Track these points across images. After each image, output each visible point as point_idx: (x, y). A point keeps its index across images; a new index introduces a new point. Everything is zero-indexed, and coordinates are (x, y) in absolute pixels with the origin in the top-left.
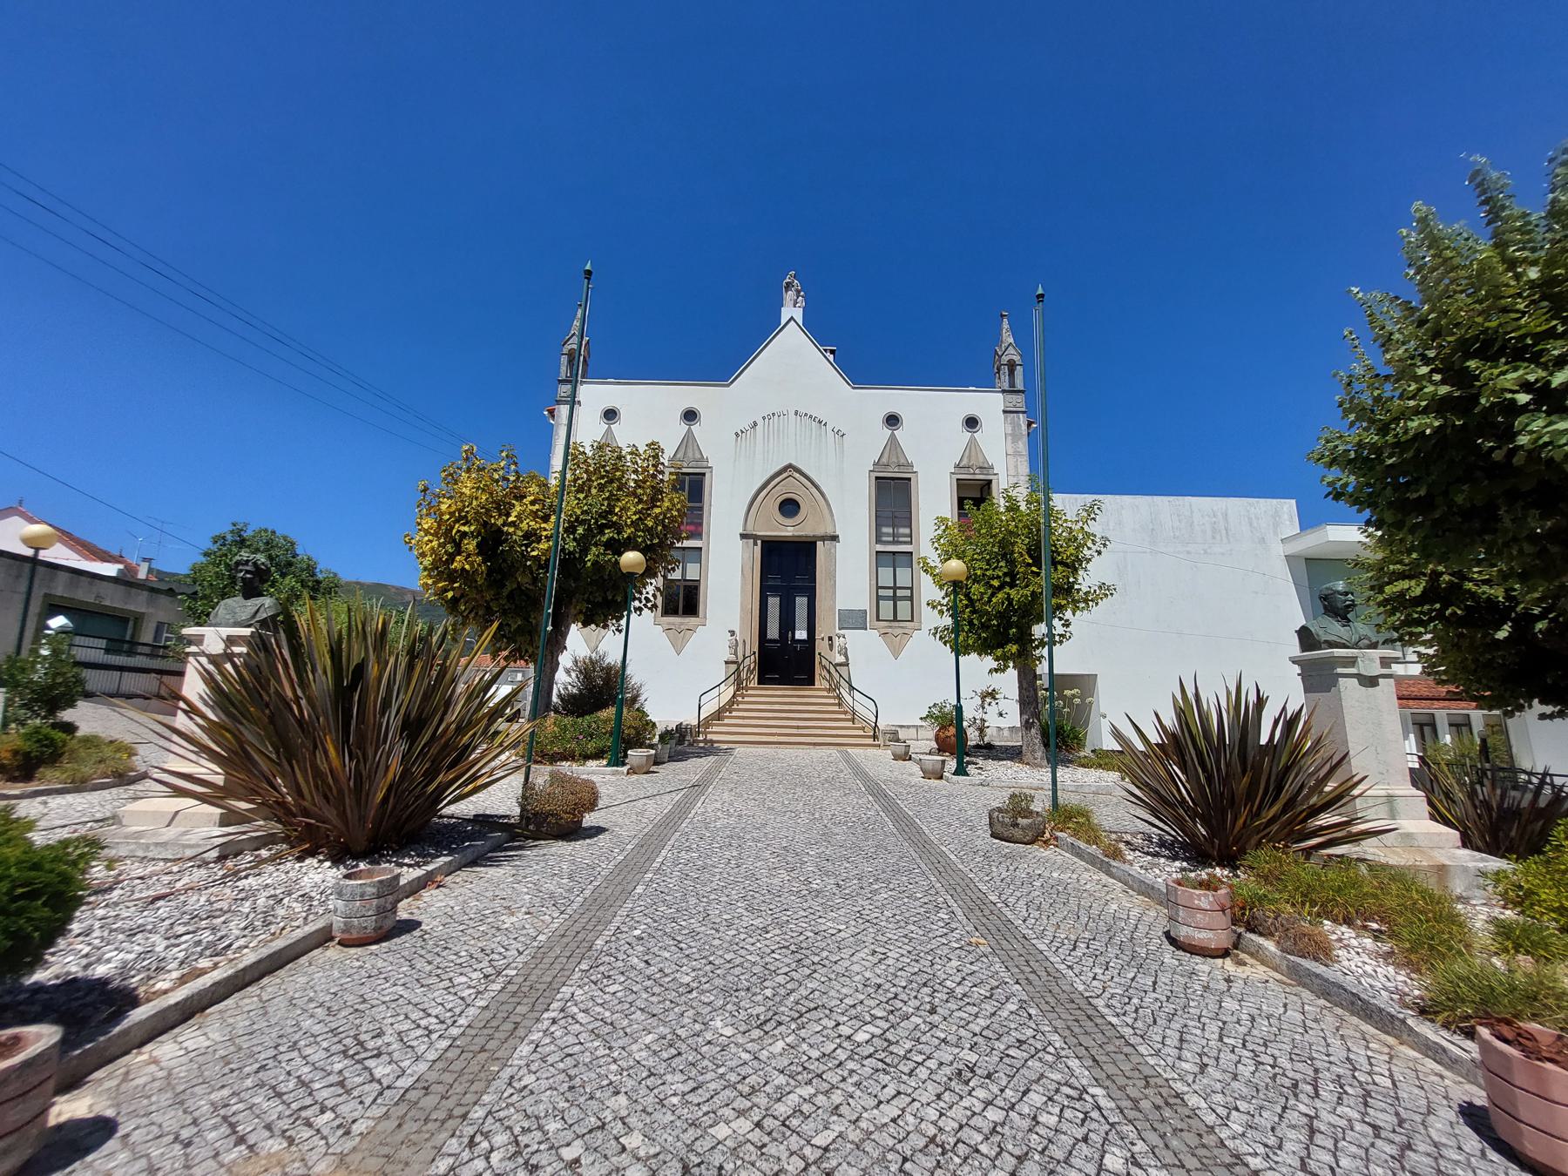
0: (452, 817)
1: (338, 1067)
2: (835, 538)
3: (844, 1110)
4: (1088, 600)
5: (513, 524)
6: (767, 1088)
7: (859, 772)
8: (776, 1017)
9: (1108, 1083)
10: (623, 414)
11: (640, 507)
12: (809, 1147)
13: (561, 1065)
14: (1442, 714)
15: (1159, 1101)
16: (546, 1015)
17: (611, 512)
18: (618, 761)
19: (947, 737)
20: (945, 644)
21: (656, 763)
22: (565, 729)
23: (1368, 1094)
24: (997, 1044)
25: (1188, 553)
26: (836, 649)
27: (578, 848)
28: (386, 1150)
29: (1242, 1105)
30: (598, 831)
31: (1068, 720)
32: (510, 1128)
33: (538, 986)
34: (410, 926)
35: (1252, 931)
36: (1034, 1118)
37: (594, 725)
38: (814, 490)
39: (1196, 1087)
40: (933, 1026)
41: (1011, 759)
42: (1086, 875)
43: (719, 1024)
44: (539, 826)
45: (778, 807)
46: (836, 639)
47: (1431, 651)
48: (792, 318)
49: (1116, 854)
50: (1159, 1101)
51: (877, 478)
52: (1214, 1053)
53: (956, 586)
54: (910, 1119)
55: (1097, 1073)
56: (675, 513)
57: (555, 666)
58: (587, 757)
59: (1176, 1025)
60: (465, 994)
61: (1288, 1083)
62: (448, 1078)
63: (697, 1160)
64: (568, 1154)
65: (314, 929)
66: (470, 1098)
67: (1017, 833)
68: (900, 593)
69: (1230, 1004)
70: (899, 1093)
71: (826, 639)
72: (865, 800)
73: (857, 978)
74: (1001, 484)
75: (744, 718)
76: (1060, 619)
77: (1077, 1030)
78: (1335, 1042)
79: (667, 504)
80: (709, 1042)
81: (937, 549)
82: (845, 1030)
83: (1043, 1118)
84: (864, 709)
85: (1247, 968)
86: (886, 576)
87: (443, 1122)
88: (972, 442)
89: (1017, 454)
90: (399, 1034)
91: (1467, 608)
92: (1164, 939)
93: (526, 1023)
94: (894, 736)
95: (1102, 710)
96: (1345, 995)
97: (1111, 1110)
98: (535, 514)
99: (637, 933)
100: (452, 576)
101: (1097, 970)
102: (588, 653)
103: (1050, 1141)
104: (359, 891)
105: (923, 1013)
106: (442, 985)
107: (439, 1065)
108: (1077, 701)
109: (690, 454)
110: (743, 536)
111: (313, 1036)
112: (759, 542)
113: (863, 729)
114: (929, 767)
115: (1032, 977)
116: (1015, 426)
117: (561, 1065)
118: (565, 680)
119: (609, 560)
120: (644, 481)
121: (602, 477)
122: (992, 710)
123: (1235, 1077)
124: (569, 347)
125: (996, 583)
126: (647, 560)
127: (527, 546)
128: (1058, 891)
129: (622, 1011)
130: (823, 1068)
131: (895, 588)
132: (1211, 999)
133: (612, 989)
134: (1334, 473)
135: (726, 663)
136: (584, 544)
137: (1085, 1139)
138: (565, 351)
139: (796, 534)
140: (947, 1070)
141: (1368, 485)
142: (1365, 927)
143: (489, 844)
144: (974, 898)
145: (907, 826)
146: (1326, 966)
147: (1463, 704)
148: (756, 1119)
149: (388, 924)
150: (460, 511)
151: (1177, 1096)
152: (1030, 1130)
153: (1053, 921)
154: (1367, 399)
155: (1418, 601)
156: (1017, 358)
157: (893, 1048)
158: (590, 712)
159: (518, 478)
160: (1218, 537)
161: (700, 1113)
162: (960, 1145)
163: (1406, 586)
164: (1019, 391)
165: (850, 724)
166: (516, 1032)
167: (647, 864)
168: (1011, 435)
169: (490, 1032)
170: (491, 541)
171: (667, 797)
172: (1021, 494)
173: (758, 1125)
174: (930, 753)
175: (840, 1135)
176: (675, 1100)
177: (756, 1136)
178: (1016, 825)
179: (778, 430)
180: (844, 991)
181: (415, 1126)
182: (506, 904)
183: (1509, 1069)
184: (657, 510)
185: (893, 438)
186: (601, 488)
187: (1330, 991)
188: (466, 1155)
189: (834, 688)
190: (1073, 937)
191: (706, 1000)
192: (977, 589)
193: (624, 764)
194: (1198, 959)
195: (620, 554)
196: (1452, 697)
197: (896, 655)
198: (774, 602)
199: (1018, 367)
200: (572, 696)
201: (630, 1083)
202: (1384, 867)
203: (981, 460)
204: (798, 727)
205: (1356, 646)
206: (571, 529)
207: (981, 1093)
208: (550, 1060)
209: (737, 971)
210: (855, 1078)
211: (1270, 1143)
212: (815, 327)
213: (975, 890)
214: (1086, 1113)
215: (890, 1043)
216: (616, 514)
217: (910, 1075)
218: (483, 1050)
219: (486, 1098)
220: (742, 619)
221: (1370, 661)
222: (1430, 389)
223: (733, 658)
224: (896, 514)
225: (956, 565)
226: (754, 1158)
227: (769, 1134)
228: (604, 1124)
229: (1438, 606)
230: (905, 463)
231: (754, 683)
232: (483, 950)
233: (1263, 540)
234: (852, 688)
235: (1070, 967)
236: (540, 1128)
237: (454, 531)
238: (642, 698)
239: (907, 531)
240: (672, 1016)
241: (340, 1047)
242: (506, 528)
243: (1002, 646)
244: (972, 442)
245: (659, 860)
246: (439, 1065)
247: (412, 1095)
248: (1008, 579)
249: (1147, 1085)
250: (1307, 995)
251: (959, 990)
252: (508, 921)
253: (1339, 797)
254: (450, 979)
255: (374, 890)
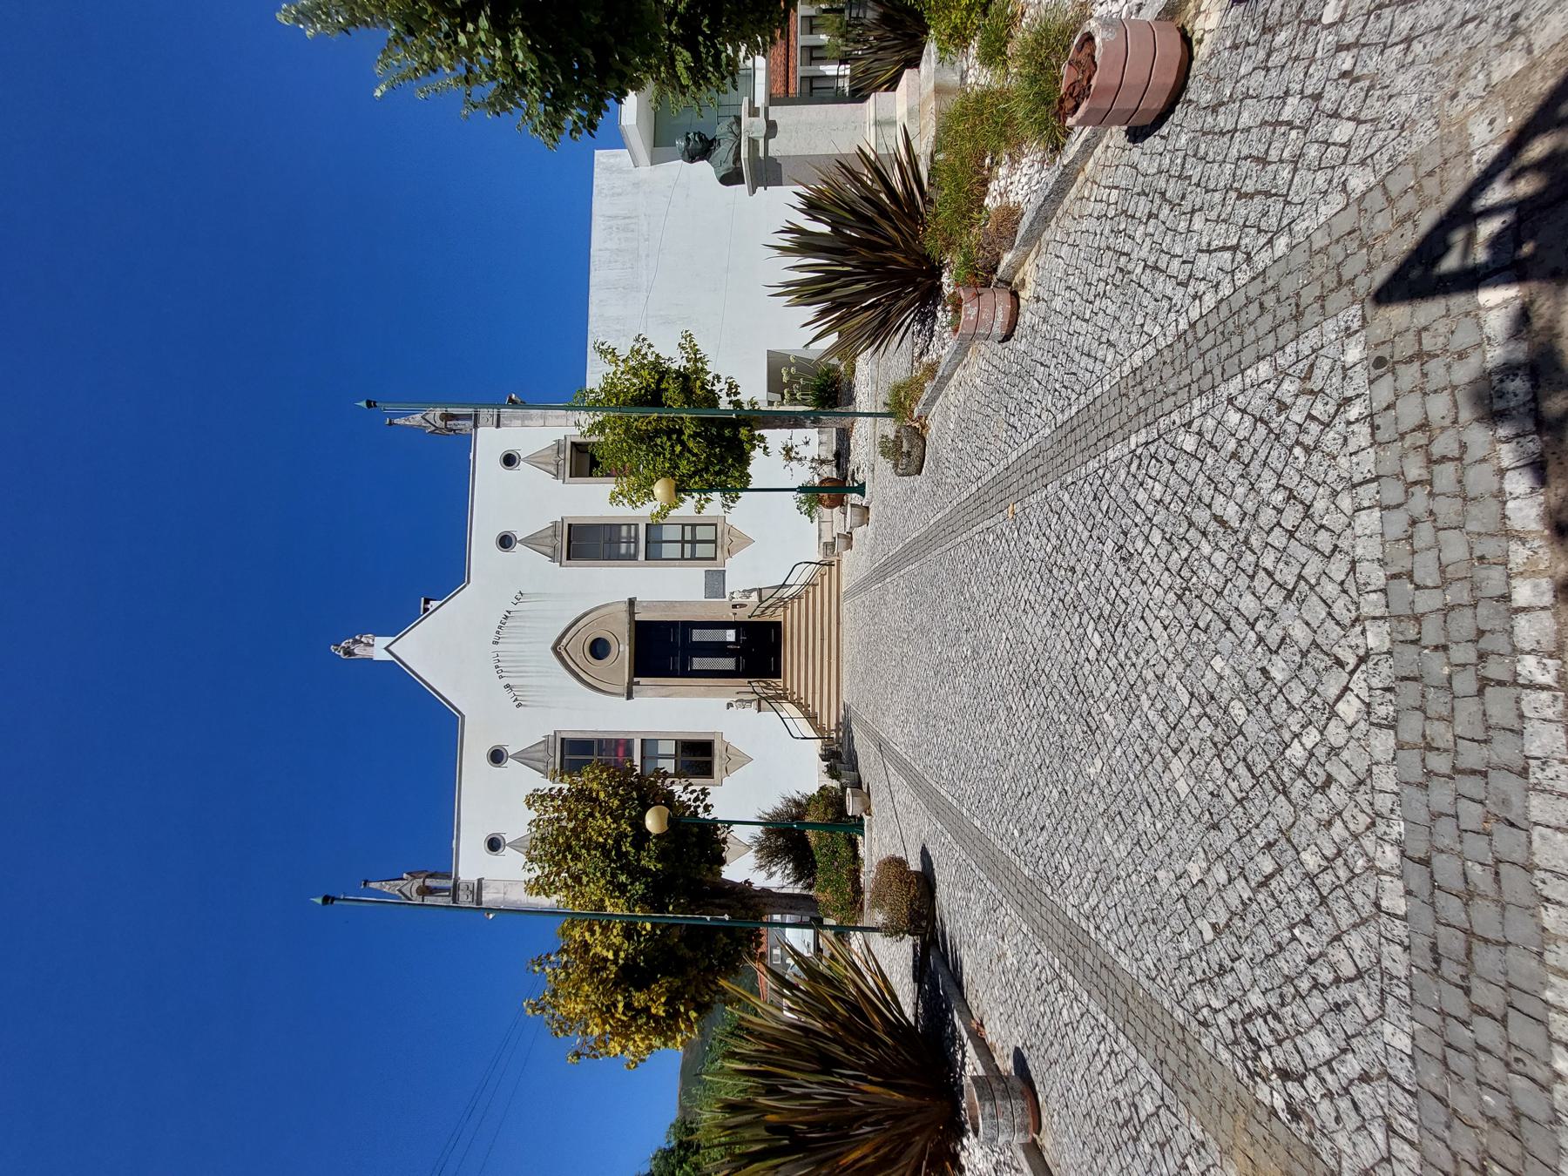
0: (916, 1004)
1: (1147, 1148)
2: (632, 602)
3: (1159, 670)
4: (696, 357)
5: (616, 954)
6: (1145, 737)
7: (862, 586)
8: (1084, 715)
9: (1126, 429)
10: (491, 830)
11: (597, 815)
12: (1192, 710)
13: (1135, 928)
14: (802, 39)
15: (1139, 389)
16: (1093, 936)
17: (603, 846)
18: (859, 824)
20: (738, 498)
21: (860, 787)
22: (829, 881)
23: (1124, 212)
24: (1097, 519)
25: (648, 256)
26: (744, 600)
27: (942, 877)
28: (1215, 1108)
29: (1139, 320)
30: (925, 854)
31: (810, 380)
32: (1190, 985)
33: (1068, 939)
34: (1019, 1059)
35: (995, 270)
36: (1158, 502)
37: (824, 851)
38: (581, 624)
39: (1126, 355)
40: (1085, 572)
41: (849, 439)
42: (952, 398)
43: (1092, 770)
44: (922, 917)
45: (899, 671)
46: (735, 601)
47: (743, 48)
48: (387, 649)
49: (932, 369)
50: (1139, 389)
51: (568, 558)
52: (1099, 331)
53: (681, 489)
54: (1163, 613)
55: (1119, 435)
56: (605, 775)
57: (766, 892)
58: (856, 857)
59: (1077, 357)
60: (1078, 1013)
61: (1119, 276)
62: (1151, 1039)
63: (1207, 815)
64: (1209, 935)
65: (1026, 1163)
66: (1167, 1021)
67: (916, 452)
68: (688, 537)
69: (1057, 304)
70: (1142, 618)
71: (735, 610)
72: (890, 586)
73: (1048, 633)
74: (575, 434)
75: (814, 693)
76: (713, 385)
77: (1084, 444)
78: (1085, 225)
79: (595, 786)
80: (1109, 783)
82: (1092, 655)
83: (1157, 495)
84: (802, 576)
85: (1028, 279)
86: (671, 550)
87: (1189, 1049)
88: (530, 460)
89: (544, 418)
90: (1116, 1083)
91: (703, 14)
92: (1005, 344)
93: (1100, 955)
94: (829, 546)
95: (800, 347)
96: (1047, 206)
97: (1147, 433)
98: (606, 929)
99: (1016, 834)
100: (673, 1015)
101: (1033, 412)
102: (751, 853)
103: (1175, 493)
104: (988, 1121)
105: (1075, 580)
106: (1071, 1034)
107: (1141, 1045)
108: (793, 370)
109: (540, 755)
110: (630, 696)
111: (1121, 1171)
112: (636, 680)
113: (822, 576)
114: (857, 519)
115: (1040, 471)
117: (1135, 928)
118: (778, 880)
119: (655, 844)
120: (570, 811)
121: (565, 857)
122: (803, 451)
123: (1116, 319)
126: (656, 804)
127: (639, 935)
128: (966, 427)
129: (1086, 861)
130: (1124, 682)
131: (683, 542)
132: (1053, 319)
133: (1067, 867)
134: (569, 120)
136: (637, 872)
137: (1173, 463)
140: (1122, 570)
141: (579, 98)
142: (990, 169)
143: (941, 969)
144: (973, 506)
145: (914, 551)
146: (1023, 214)
147: (792, 19)
148: (1171, 754)
149: (1018, 1084)
150: (602, 1013)
151: (1134, 372)
152: (1167, 508)
153: (992, 440)
154: (491, 88)
155: (696, 56)
156: (439, 411)
157: (1106, 613)
158: (812, 855)
159: (566, 951)
160: (632, 226)
161: (1169, 804)
162: (1182, 573)
163: (682, 64)
165: (818, 588)
166: (1110, 968)
167: (954, 811)
169: (1110, 993)
170: (633, 976)
171: (892, 779)
172: (586, 419)
173: (1175, 752)
174: (845, 514)
175: (1180, 679)
176: (1159, 826)
177: (1185, 755)
178: (909, 454)
180: (1059, 647)
181: (1194, 1077)
182: (995, 960)
183: (1098, 111)
184: (602, 795)
186: (577, 857)
187: (1044, 217)
188: (1215, 1032)
190: (1005, 426)
191: (1073, 778)
192: (684, 467)
193: (861, 819)
194: (1021, 320)
195: (650, 833)
196: (786, 35)
197: (749, 541)
198: (698, 663)
200: (795, 869)
201: (1147, 865)
202: (937, 139)
203: (550, 452)
204: (822, 639)
205: (738, 137)
206: (622, 888)
207: (1140, 544)
208: (1131, 938)
209: (1047, 745)
210: (1132, 654)
211: (1167, 306)
212: (398, 621)
213: (967, 503)
214: (1152, 457)
215: (1101, 615)
216: (606, 840)
217: (1127, 604)
218: (1125, 1002)
219: (1167, 1005)
221: (753, 127)
222: (482, 36)
223: (754, 704)
224: (607, 539)
225: (660, 489)
226: (1203, 763)
227: (1182, 744)
228: (1182, 896)
229: (701, 39)
231: (780, 682)
232: (1038, 989)
233: (636, 185)
235: (1031, 435)
236: (1189, 957)
237: (624, 1018)
238: (797, 797)
239: (624, 529)
240: (1088, 813)
241: (1130, 1143)
242: (621, 962)
244: (530, 460)
245: (950, 799)
246: (1141, 1045)
247: (1168, 1076)
248: (674, 437)
249: (1126, 395)
250: (1047, 235)
251: (1054, 541)
252: (1011, 960)
253: (877, 170)
254: (1066, 1025)
255: (987, 1104)
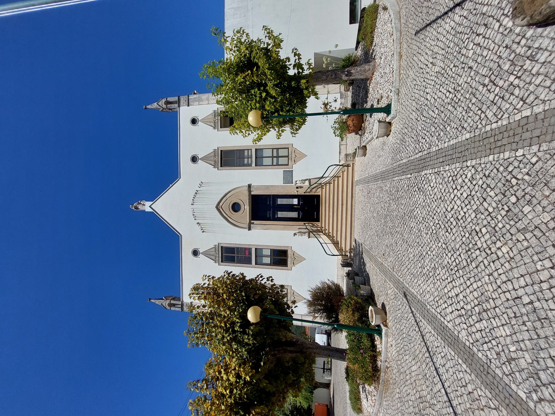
19: (353, 125)
26: (302, 185)
38: (228, 196)
48: (150, 207)
71: (297, 190)
81: (249, 134)
84: (332, 172)
86: (267, 161)
109: (213, 253)
110: (250, 229)
112: (252, 221)
114: (383, 131)
116: (195, 100)
124: (167, 306)
125: (264, 95)
131: (273, 157)
135: (309, 237)
138: (169, 308)
139: (248, 204)
156: (164, 100)
164: (179, 99)
165: (340, 179)
168: (199, 102)
179: (201, 213)
185: (202, 159)
189: (321, 186)
198: (280, 214)
199: (168, 100)
203: (211, 116)
204: (342, 205)
212: (153, 196)
220: (288, 230)
223: (307, 234)
230: (214, 153)
231: (319, 224)
234: (322, 177)
239: (246, 152)
243: (302, 90)
248: (262, 88)
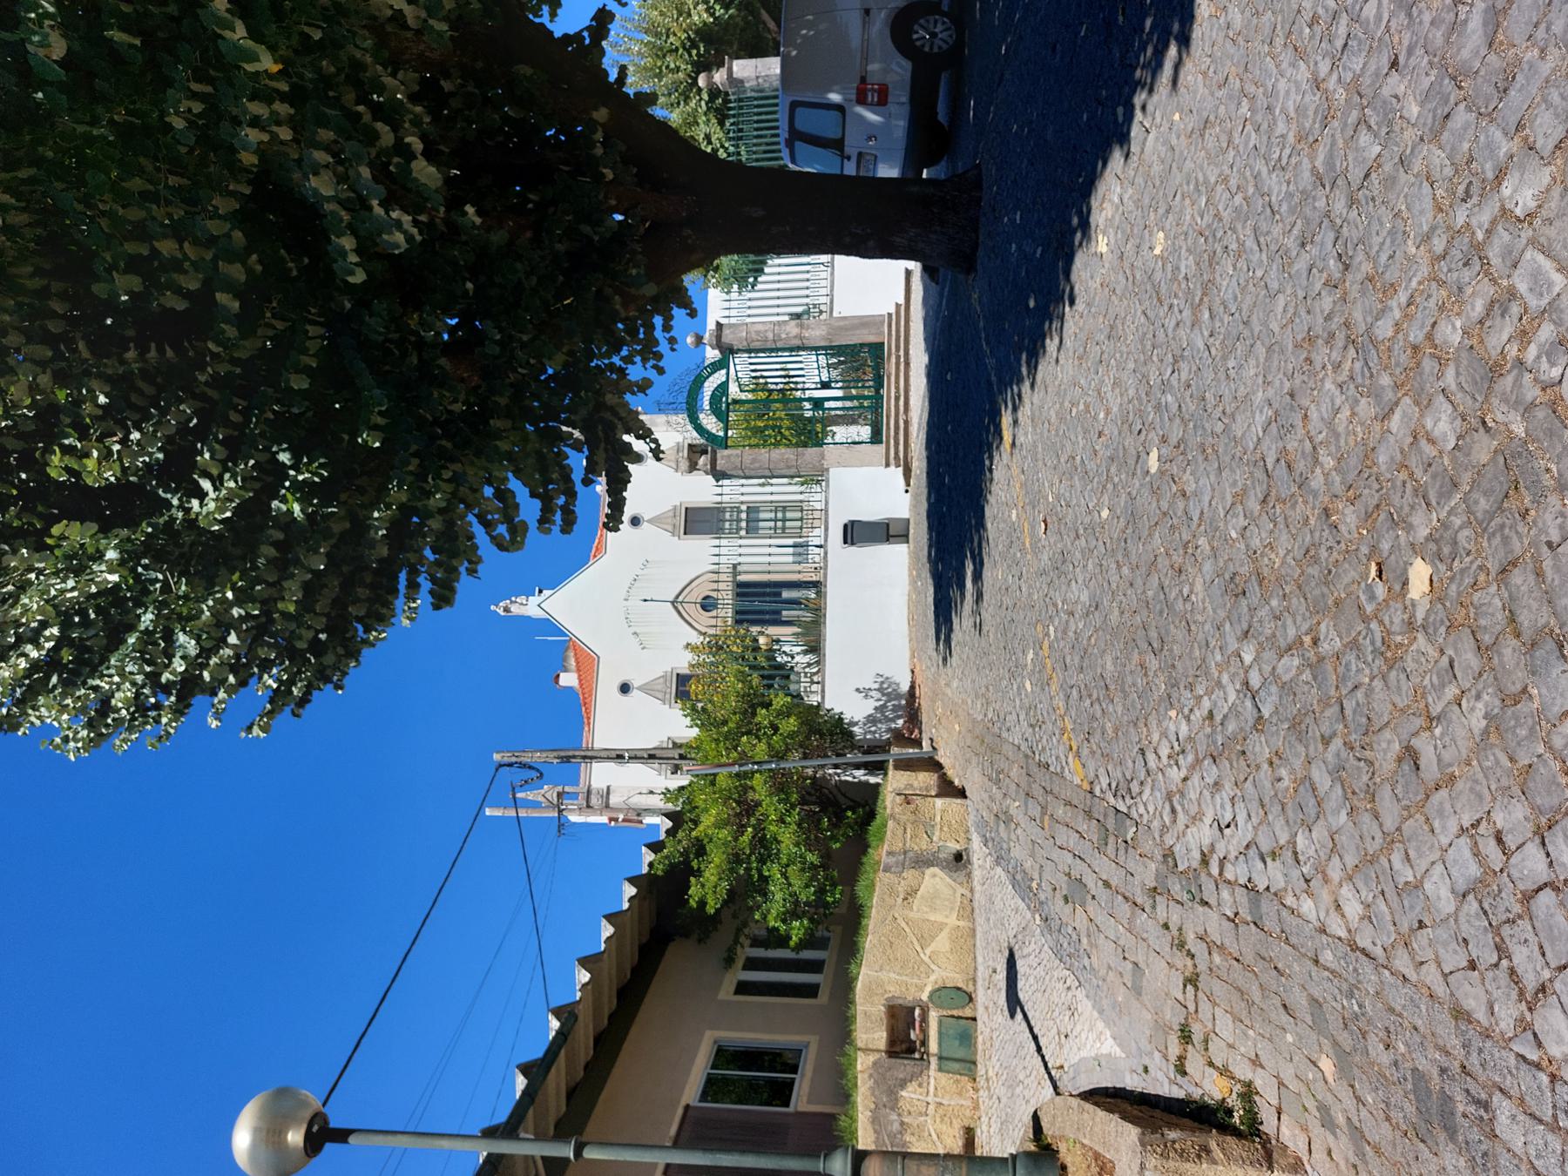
38: (693, 584)
60: (1189, 836)
109: (659, 687)
